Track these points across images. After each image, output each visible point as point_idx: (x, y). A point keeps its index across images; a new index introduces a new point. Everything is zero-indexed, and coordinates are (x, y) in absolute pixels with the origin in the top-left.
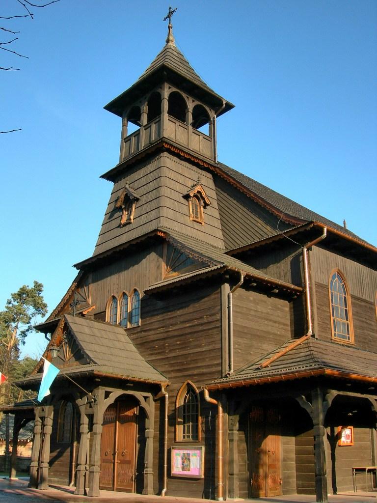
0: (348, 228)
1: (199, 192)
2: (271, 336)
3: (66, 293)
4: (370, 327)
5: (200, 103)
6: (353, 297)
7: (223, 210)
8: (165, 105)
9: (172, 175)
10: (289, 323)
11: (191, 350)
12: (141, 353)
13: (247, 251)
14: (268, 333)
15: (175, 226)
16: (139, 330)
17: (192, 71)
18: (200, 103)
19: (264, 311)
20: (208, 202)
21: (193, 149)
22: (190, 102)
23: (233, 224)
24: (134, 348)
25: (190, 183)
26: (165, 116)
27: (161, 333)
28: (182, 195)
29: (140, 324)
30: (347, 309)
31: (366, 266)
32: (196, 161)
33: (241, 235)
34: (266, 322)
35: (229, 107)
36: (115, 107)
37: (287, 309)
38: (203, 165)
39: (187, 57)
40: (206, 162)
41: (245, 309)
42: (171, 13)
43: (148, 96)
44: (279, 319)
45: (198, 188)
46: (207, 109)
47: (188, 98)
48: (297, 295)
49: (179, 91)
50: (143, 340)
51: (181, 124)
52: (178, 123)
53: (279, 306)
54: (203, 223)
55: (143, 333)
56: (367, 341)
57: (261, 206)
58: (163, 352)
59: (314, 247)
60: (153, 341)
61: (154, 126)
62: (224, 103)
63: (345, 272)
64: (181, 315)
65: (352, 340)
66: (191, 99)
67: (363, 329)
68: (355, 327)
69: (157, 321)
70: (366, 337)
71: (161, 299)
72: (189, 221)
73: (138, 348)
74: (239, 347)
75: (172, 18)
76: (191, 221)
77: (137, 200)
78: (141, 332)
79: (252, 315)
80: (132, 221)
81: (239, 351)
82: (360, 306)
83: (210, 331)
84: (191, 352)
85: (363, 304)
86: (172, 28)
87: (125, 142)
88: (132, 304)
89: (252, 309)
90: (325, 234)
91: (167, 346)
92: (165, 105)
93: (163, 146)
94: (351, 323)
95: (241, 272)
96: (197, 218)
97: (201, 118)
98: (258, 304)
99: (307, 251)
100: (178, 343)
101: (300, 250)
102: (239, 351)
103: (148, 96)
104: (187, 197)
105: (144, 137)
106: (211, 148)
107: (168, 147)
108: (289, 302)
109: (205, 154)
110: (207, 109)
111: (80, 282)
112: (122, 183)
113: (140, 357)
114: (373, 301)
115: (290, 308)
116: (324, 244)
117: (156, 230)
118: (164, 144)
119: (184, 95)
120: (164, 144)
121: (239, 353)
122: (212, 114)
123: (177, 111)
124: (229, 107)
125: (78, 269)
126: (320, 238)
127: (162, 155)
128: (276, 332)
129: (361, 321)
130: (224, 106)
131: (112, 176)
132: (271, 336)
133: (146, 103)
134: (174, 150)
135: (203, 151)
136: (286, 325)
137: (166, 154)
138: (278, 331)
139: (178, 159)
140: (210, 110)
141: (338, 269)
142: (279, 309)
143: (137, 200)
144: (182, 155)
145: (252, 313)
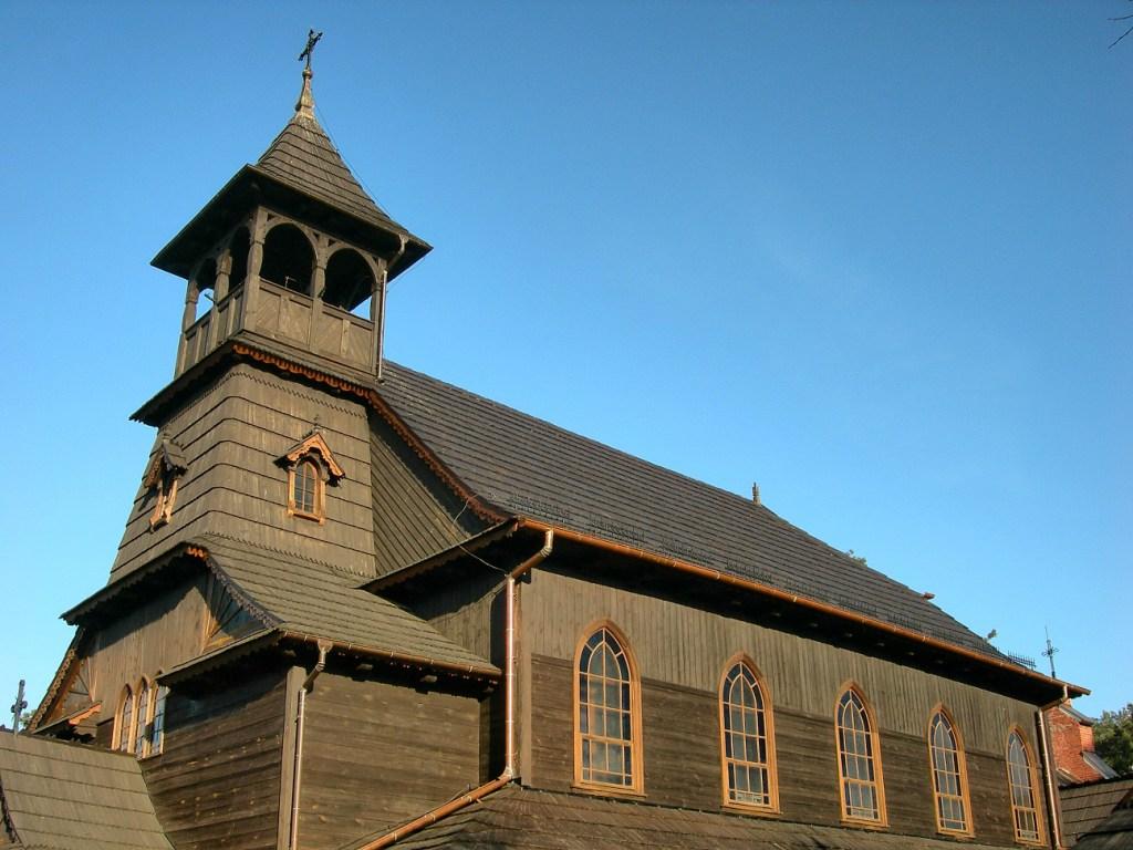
0: (763, 501)
1: (313, 450)
2: (420, 782)
3: (54, 675)
4: (699, 751)
5: (348, 246)
6: (646, 682)
7: (379, 487)
8: (256, 257)
9: (251, 414)
10: (476, 748)
11: (235, 814)
12: (159, 815)
13: (403, 583)
14: (414, 774)
15: (244, 532)
16: (160, 762)
17: (345, 175)
18: (348, 246)
19: (404, 723)
20: (336, 472)
21: (322, 351)
22: (321, 244)
23: (394, 518)
24: (146, 802)
25: (298, 431)
26: (254, 281)
27: (187, 773)
28: (275, 459)
29: (161, 751)
30: (630, 712)
31: (699, 608)
32: (318, 380)
33: (405, 545)
34: (408, 750)
35: (417, 250)
36: (174, 258)
37: (474, 717)
38: (339, 388)
39: (337, 144)
40: (343, 381)
41: (346, 723)
42: (312, 43)
43: (231, 235)
44: (446, 742)
45: (312, 442)
46: (368, 257)
47: (317, 236)
48: (492, 686)
49: (295, 222)
50: (164, 786)
51: (293, 296)
52: (287, 296)
53: (450, 712)
54: (322, 520)
55: (165, 770)
56: (686, 785)
57: (440, 478)
58: (191, 815)
59: (535, 572)
60: (179, 789)
61: (233, 303)
62: (403, 242)
63: (629, 625)
64: (223, 735)
65: (638, 785)
66: (325, 239)
67: (676, 757)
68: (649, 753)
69: (185, 746)
70: (685, 776)
71: (196, 697)
72: (283, 516)
73: (155, 804)
74: (323, 810)
75: (312, 53)
76: (290, 517)
77: (182, 471)
78: (161, 767)
79: (368, 736)
80: (168, 519)
81: (323, 818)
82: (671, 704)
83: (264, 773)
84: (232, 818)
85: (680, 697)
86: (310, 77)
87: (188, 339)
88: (151, 706)
89: (367, 723)
90: (548, 546)
91: (199, 802)
92: (256, 257)
93: (234, 351)
94: (637, 745)
95: (319, 642)
96: (307, 508)
97: (350, 286)
98: (386, 710)
99: (516, 584)
100: (215, 795)
101: (501, 585)
102: (323, 818)
103: (231, 235)
104: (283, 463)
105: (216, 328)
106: (372, 345)
107: (247, 352)
108: (480, 701)
109: (352, 362)
110: (368, 257)
111: (82, 649)
112: (174, 427)
113: (153, 821)
114: (711, 690)
115: (482, 715)
116: (552, 564)
117: (183, 545)
118: (236, 347)
119: (306, 230)
120: (236, 347)
121: (324, 822)
122: (380, 269)
123: (288, 267)
124: (417, 250)
125: (70, 623)
126: (538, 555)
127: (234, 370)
128: (435, 771)
129: (668, 738)
130: (403, 248)
131: (156, 412)
132: (420, 782)
133: (228, 251)
134: (262, 357)
135: (348, 352)
136: (469, 754)
137: (243, 368)
138: (440, 768)
139: (276, 377)
140: (376, 260)
141: (608, 621)
142: (448, 718)
143: (182, 471)
144: (282, 367)
145: (369, 730)
